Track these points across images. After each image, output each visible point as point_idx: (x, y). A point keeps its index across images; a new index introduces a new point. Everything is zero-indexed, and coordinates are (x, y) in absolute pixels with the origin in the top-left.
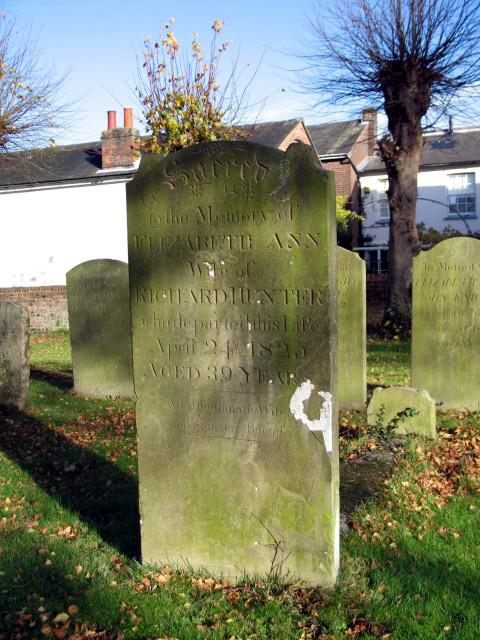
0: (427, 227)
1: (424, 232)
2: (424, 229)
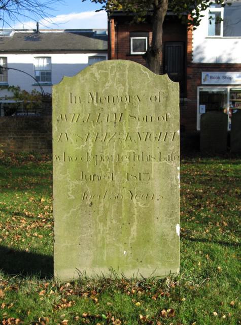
0: (22, 89)
1: (20, 93)
2: (20, 91)
